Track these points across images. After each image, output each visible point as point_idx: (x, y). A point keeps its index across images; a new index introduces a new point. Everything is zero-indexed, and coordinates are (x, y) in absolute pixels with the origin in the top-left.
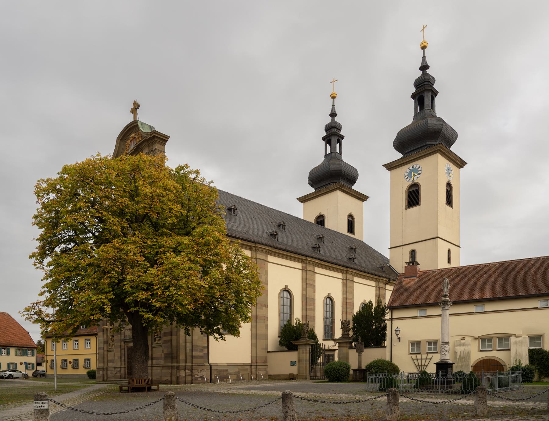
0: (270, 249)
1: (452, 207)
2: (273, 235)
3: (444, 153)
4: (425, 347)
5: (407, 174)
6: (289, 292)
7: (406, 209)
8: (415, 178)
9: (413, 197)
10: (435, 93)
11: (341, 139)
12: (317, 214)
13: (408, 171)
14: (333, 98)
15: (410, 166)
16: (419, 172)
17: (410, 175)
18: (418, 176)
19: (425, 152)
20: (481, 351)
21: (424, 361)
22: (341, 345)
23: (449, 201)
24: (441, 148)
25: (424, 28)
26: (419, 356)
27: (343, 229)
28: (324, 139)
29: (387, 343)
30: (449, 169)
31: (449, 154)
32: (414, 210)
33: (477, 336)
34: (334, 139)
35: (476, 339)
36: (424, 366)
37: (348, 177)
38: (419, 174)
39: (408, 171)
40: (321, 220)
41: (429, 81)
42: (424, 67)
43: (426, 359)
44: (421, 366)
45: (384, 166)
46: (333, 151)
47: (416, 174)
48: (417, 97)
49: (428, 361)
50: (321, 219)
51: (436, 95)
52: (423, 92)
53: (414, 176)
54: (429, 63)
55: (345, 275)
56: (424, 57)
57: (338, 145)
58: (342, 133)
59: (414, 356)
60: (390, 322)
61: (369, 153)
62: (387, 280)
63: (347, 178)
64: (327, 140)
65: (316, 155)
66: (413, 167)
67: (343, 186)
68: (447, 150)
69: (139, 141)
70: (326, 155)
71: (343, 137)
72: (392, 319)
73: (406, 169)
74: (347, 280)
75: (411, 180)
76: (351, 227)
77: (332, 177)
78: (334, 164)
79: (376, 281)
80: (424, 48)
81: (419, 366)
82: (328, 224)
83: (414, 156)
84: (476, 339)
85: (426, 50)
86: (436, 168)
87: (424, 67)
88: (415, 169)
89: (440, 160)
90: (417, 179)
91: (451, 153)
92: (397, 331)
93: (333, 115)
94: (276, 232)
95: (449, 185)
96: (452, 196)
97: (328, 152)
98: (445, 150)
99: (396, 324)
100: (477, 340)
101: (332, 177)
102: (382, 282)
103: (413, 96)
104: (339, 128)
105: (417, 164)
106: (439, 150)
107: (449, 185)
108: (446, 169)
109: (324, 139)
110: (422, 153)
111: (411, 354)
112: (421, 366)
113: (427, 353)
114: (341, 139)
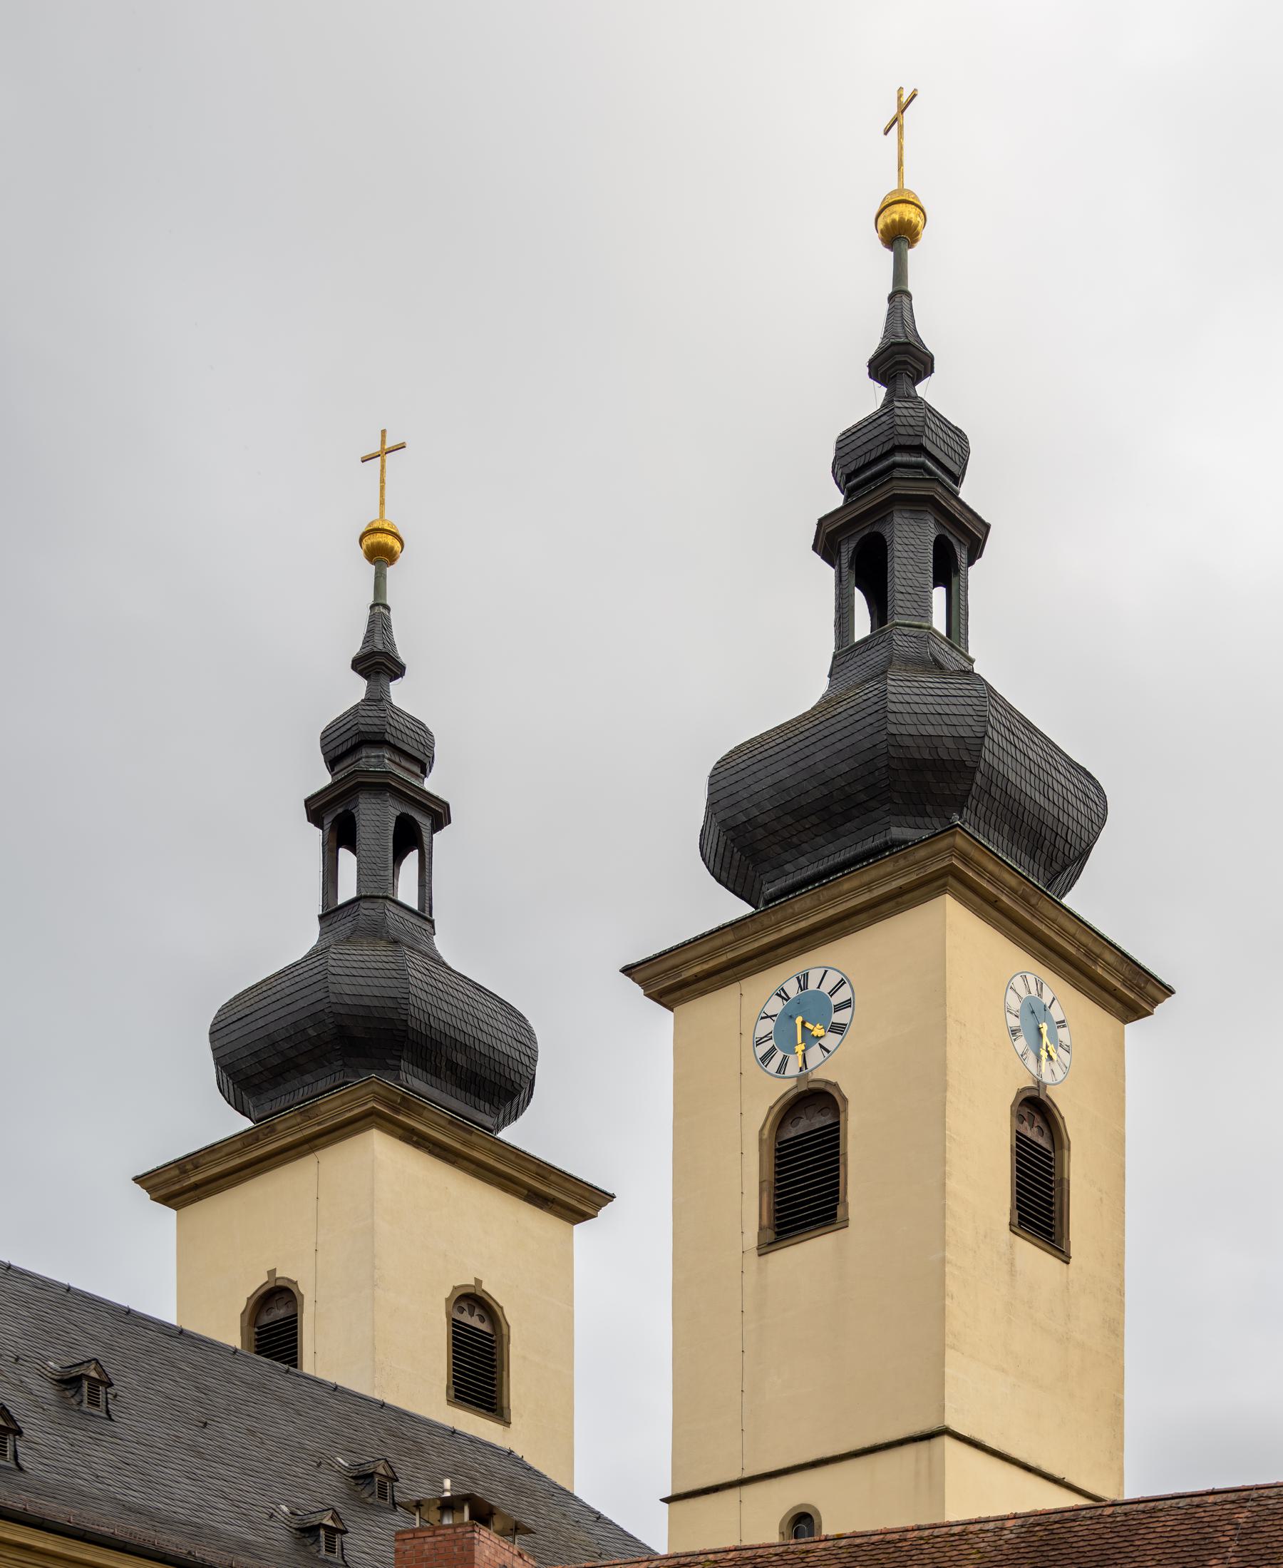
1: (1064, 1255)
3: (994, 903)
5: (767, 1027)
7: (765, 1248)
8: (815, 1055)
9: (805, 1178)
11: (424, 822)
13: (776, 1006)
14: (380, 556)
15: (784, 976)
16: (838, 1017)
17: (784, 1035)
18: (831, 1040)
19: (868, 886)
23: (1039, 1206)
24: (965, 858)
25: (903, 108)
27: (418, 1381)
28: (317, 809)
30: (1034, 1011)
32: (812, 1252)
34: (376, 818)
37: (460, 1059)
38: (838, 1029)
39: (776, 1006)
40: (275, 1322)
41: (921, 449)
42: (900, 361)
46: (376, 893)
47: (818, 1031)
50: (280, 1312)
51: (975, 550)
52: (883, 511)
53: (810, 1039)
54: (930, 330)
56: (899, 296)
57: (939, 596)
58: (431, 784)
61: (565, 895)
63: (453, 1066)
64: (334, 816)
65: (267, 910)
66: (803, 982)
67: (406, 1104)
70: (331, 914)
71: (440, 815)
73: (762, 995)
75: (793, 1068)
76: (478, 1363)
77: (365, 1049)
78: (364, 973)
80: (898, 236)
82: (325, 1352)
83: (805, 913)
85: (390, 571)
86: (935, 994)
87: (900, 361)
88: (817, 994)
89: (957, 940)
90: (830, 1063)
93: (378, 663)
94: (336, 1516)
95: (1035, 1107)
96: (1063, 1184)
97: (347, 890)
101: (365, 1049)
104: (418, 753)
105: (824, 966)
106: (952, 872)
108: (1015, 1004)
109: (317, 809)
110: (852, 890)
114: (424, 822)
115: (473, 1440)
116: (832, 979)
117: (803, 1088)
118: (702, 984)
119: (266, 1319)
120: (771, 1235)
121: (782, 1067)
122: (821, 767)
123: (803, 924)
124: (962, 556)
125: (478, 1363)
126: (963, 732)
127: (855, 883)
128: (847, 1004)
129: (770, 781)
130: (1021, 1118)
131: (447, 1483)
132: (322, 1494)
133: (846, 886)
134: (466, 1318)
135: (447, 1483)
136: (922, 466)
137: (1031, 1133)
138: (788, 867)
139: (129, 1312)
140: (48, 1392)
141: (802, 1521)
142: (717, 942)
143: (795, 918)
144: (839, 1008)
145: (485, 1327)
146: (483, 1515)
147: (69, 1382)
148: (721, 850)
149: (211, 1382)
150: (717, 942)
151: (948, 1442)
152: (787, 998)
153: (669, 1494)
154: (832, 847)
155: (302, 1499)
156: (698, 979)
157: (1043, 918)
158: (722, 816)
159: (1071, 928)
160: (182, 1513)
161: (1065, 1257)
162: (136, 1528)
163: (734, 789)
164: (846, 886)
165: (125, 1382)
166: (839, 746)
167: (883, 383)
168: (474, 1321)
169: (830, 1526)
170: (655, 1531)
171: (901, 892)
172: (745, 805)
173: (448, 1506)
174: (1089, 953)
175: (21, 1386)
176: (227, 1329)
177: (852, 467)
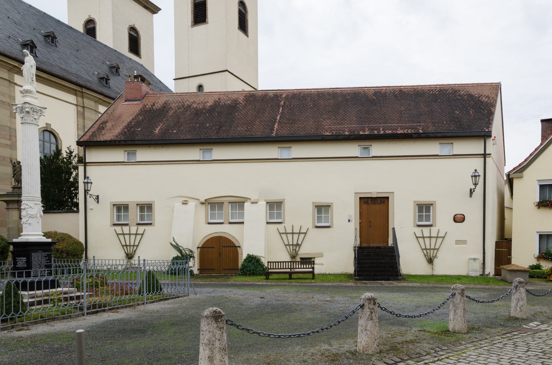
0: (101, 97)
1: (247, 36)
2: (105, 80)
4: (134, 214)
6: (52, 133)
12: (85, 18)
21: (133, 237)
22: (11, 206)
23: (243, 25)
26: (126, 229)
27: (124, 48)
32: (201, 28)
33: (203, 200)
35: (202, 203)
36: (134, 246)
43: (136, 234)
44: (130, 246)
50: (91, 26)
55: (80, 99)
59: (119, 229)
69: (89, 16)
74: (84, 107)
76: (134, 44)
79: (76, 95)
81: (126, 246)
84: (202, 203)
94: (107, 76)
96: (247, 20)
100: (204, 205)
112: (293, 245)
113: (138, 224)
115: (135, 61)
119: (89, 27)
120: (193, 23)
125: (134, 44)
130: (239, 5)
131: (135, 72)
132: (104, 71)
134: (131, 33)
135: (135, 72)
137: (242, 9)
139: (59, 21)
140: (42, 39)
141: (200, 87)
145: (135, 35)
146: (143, 80)
147: (46, 36)
149: (79, 41)
151: (227, 72)
152: (130, 257)
155: (100, 71)
160: (74, 72)
161: (247, 36)
162: (64, 74)
165: (59, 38)
168: (133, 33)
169: (206, 89)
170: (171, 85)
173: (136, 77)
175: (35, 36)
176: (80, 27)
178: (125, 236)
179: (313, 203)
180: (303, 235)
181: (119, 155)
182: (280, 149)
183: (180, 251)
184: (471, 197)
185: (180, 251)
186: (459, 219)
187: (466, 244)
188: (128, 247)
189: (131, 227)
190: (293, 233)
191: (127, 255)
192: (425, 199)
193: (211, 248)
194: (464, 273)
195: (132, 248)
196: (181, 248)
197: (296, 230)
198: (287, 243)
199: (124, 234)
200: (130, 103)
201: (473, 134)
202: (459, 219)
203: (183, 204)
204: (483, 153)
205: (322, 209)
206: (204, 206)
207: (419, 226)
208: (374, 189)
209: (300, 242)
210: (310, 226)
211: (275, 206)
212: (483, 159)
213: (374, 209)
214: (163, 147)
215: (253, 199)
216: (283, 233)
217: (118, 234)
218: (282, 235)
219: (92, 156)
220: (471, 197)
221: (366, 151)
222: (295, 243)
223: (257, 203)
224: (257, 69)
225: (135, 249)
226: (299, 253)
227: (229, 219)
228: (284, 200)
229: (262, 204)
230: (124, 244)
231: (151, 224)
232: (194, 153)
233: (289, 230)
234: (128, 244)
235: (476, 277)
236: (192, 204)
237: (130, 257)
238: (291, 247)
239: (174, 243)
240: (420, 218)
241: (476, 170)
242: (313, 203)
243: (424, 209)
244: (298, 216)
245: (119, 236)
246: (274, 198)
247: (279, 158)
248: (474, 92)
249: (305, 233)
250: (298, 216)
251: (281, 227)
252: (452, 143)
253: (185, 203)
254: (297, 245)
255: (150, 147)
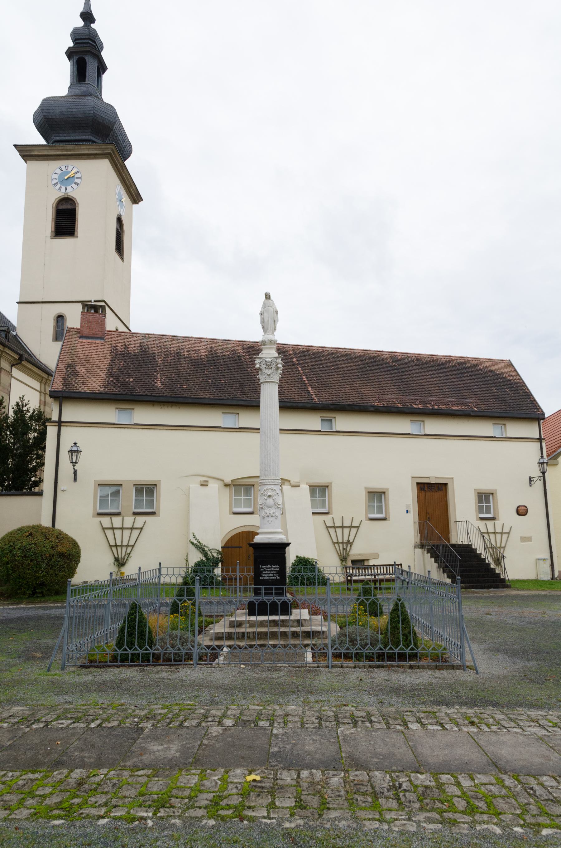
4: (128, 499)
5: (55, 176)
9: (65, 220)
10: (102, 68)
15: (62, 164)
19: (88, 149)
20: (235, 513)
23: (119, 248)
26: (117, 522)
29: (47, 486)
31: (123, 170)
32: (65, 242)
33: (228, 480)
35: (226, 485)
36: (127, 546)
39: (59, 171)
43: (132, 529)
45: (16, 146)
48: (75, 58)
49: (505, 536)
59: (106, 521)
60: (56, 428)
62: (17, 357)
68: (121, 162)
72: (60, 423)
73: (54, 168)
81: (116, 546)
83: (70, 150)
84: (226, 485)
87: (88, 16)
90: (72, 191)
91: (125, 170)
92: (75, 452)
96: (123, 241)
98: (119, 162)
99: (70, 436)
100: (228, 488)
102: (7, 360)
103: (70, 54)
107: (119, 220)
110: (84, 149)
111: (100, 514)
112: (343, 543)
113: (135, 514)
116: (75, 170)
117: (66, 196)
118: (37, 158)
120: (54, 234)
121: (60, 188)
122: (74, 113)
123: (69, 153)
124: (102, 73)
126: (111, 120)
127: (85, 147)
128: (79, 178)
129: (60, 110)
133: (82, 147)
136: (94, 46)
138: (61, 135)
142: (44, 148)
143: (67, 150)
144: (77, 178)
148: (41, 122)
150: (44, 148)
152: (120, 563)
153: (18, 301)
154: (74, 134)
156: (36, 156)
157: (124, 173)
158: (45, 114)
159: (129, 177)
163: (49, 108)
164: (82, 147)
166: (80, 110)
167: (84, 21)
171: (96, 154)
172: (52, 114)
174: (131, 185)
177: (77, 37)
178: (116, 531)
179: (365, 488)
180: (356, 530)
181: (108, 413)
182: (117, 410)
183: (205, 553)
184: (531, 486)
185: (205, 553)
186: (522, 511)
187: (531, 541)
188: (119, 549)
189: (125, 518)
190: (343, 527)
191: (117, 560)
192: (485, 487)
193: (237, 547)
194: (532, 576)
195: (124, 549)
196: (206, 549)
197: (347, 523)
198: (335, 541)
199: (113, 529)
200: (89, 341)
201: (524, 416)
202: (522, 511)
203: (202, 485)
204: (538, 437)
205: (377, 496)
206: (228, 489)
207: (482, 519)
208: (433, 474)
209: (351, 540)
210: (363, 518)
211: (319, 490)
212: (539, 443)
213: (433, 496)
214: (172, 406)
215: (294, 481)
216: (331, 527)
217: (104, 529)
218: (330, 529)
219: (71, 412)
220: (531, 486)
221: (327, 424)
222: (345, 540)
223: (299, 486)
224: (129, 302)
225: (128, 551)
226: (351, 553)
227: (96, 509)
228: (331, 483)
229: (305, 489)
230: (112, 543)
231: (153, 514)
232: (403, 425)
233: (338, 524)
234: (119, 543)
235: (548, 581)
236: (214, 486)
237: (120, 563)
238: (341, 545)
239: (195, 542)
240: (480, 510)
241: (75, 444)
242: (365, 488)
243: (484, 498)
244: (349, 505)
245: (106, 531)
246: (319, 480)
247: (116, 423)
248: (494, 368)
249: (358, 527)
250: (349, 505)
251: (327, 518)
252: (238, 414)
253: (204, 484)
254: (348, 542)
255: (153, 405)
